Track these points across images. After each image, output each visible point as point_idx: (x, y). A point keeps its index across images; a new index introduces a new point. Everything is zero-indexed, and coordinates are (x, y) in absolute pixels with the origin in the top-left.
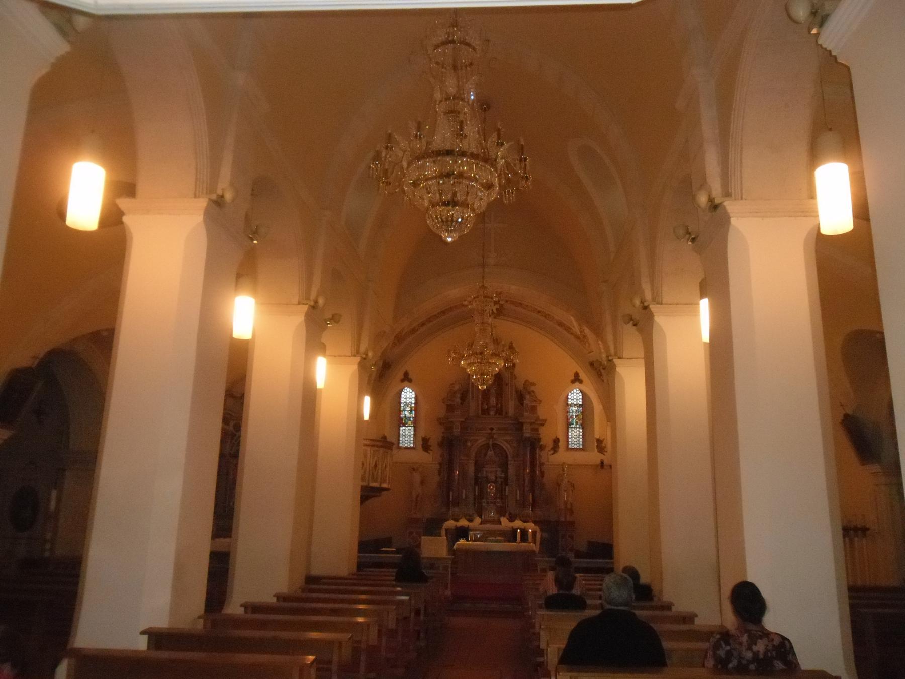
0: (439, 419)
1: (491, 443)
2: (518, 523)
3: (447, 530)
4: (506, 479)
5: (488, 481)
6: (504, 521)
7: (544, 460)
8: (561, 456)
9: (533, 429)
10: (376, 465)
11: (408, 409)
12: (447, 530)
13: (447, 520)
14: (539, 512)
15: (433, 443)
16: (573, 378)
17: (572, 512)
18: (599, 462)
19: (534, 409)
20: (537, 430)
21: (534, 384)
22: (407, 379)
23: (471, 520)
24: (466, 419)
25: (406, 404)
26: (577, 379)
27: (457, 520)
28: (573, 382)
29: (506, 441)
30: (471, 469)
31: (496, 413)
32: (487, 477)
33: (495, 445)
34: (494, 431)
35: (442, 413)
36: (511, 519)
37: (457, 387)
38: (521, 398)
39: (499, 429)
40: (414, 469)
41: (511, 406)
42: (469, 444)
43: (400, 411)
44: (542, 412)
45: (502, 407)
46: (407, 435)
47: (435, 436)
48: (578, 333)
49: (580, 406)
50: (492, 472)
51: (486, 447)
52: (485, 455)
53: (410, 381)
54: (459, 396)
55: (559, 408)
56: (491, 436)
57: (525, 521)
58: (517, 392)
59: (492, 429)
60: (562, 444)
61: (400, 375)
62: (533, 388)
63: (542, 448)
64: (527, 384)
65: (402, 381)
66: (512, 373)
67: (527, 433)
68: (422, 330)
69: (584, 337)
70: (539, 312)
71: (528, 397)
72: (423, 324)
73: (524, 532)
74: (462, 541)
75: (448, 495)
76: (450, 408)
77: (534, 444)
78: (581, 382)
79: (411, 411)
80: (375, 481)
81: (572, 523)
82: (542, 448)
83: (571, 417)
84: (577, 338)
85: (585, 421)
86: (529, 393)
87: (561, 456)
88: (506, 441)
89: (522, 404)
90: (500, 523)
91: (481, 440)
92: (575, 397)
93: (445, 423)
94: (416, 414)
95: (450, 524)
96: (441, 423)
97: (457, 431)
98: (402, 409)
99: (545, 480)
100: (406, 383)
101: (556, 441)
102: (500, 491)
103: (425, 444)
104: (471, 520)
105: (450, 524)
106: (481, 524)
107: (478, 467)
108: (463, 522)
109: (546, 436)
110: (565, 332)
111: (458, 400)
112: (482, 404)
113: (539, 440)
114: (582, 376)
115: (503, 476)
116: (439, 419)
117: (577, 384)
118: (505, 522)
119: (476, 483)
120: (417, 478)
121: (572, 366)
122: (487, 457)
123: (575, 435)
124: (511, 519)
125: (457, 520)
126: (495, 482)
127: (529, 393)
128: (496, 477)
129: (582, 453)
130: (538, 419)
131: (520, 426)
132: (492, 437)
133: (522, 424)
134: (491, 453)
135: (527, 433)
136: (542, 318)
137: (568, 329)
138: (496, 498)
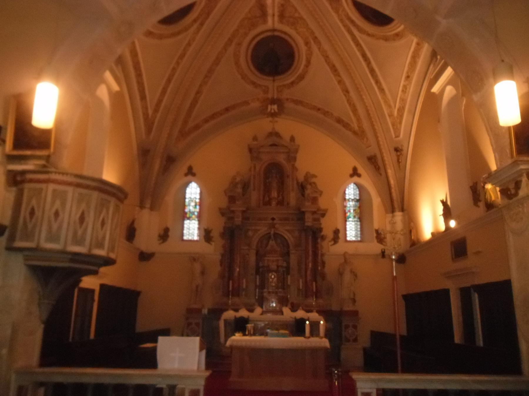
0: (220, 209)
1: (272, 232)
2: (300, 314)
3: (225, 321)
4: (288, 270)
5: (270, 271)
6: (286, 310)
7: (324, 251)
8: (339, 248)
9: (315, 220)
10: (82, 219)
11: (193, 204)
12: (225, 321)
13: (227, 310)
14: (321, 301)
15: (215, 234)
16: (351, 172)
17: (354, 301)
18: (379, 252)
19: (315, 200)
20: (318, 220)
21: (314, 176)
22: (191, 173)
23: (251, 310)
24: (248, 209)
25: (191, 200)
26: (355, 173)
27: (236, 310)
28: (352, 176)
29: (286, 230)
30: (252, 259)
31: (277, 204)
32: (268, 266)
33: (277, 236)
34: (275, 222)
35: (224, 203)
36: (294, 309)
37: (238, 179)
38: (302, 187)
39: (281, 220)
40: (194, 260)
41: (293, 198)
42: (250, 233)
43: (184, 206)
44: (322, 203)
45: (283, 198)
46: (191, 230)
47: (218, 225)
48: (356, 128)
49: (358, 201)
50: (272, 261)
51: (268, 237)
52: (267, 245)
53: (194, 175)
54: (239, 186)
55: (338, 201)
56: (273, 226)
57: (308, 311)
58: (298, 183)
59: (273, 219)
60: (341, 235)
61: (185, 170)
62: (314, 180)
63: (323, 238)
64: (308, 176)
65: (186, 175)
66: (293, 166)
67: (309, 223)
68: (207, 126)
69: (363, 132)
70: (319, 109)
71: (309, 187)
72: (206, 121)
73: (315, 325)
74: (238, 337)
75: (230, 286)
76: (232, 199)
77: (315, 234)
78: (359, 176)
79: (196, 205)
80: (79, 242)
81: (355, 313)
82: (323, 238)
83: (349, 211)
84: (355, 133)
85: (363, 214)
86: (310, 184)
87: (339, 248)
88: (288, 231)
89: (303, 195)
90: (282, 313)
91: (263, 230)
92: (351, 192)
93: (226, 213)
94: (200, 209)
95: (230, 314)
96: (223, 214)
97: (238, 221)
98: (187, 203)
99: (327, 270)
100: (190, 177)
101: (336, 232)
102: (283, 284)
103: (207, 235)
104: (251, 310)
105: (230, 314)
106: (262, 314)
107: (259, 256)
108: (243, 313)
109: (327, 226)
110: (343, 129)
111: (239, 190)
112: (264, 196)
113: (320, 230)
114: (361, 170)
115: (285, 264)
116: (220, 209)
117: (356, 178)
118: (288, 314)
119: (257, 272)
120: (197, 267)
121: (349, 160)
122: (269, 248)
123: (352, 230)
124: (294, 309)
125: (236, 310)
126: (277, 271)
127: (310, 184)
128: (278, 266)
129: (361, 244)
130: (319, 209)
131: (301, 215)
132: (274, 227)
133: (303, 213)
134: (272, 243)
135: (309, 223)
136: (321, 116)
137: (346, 126)
138: (277, 288)
